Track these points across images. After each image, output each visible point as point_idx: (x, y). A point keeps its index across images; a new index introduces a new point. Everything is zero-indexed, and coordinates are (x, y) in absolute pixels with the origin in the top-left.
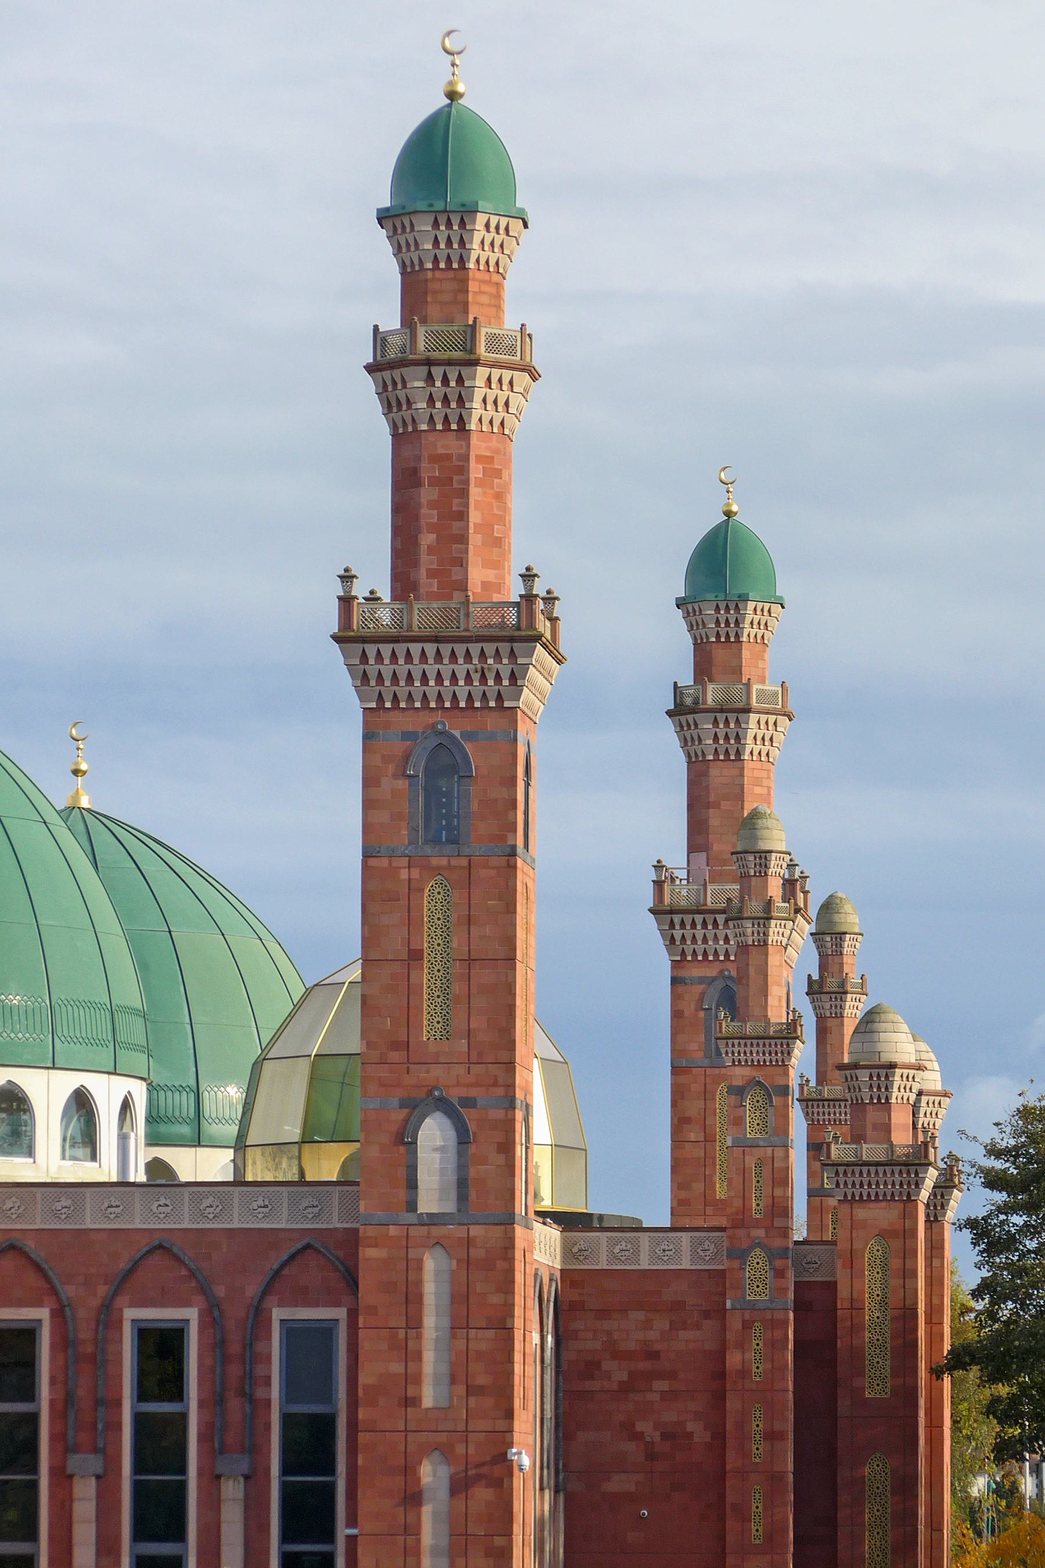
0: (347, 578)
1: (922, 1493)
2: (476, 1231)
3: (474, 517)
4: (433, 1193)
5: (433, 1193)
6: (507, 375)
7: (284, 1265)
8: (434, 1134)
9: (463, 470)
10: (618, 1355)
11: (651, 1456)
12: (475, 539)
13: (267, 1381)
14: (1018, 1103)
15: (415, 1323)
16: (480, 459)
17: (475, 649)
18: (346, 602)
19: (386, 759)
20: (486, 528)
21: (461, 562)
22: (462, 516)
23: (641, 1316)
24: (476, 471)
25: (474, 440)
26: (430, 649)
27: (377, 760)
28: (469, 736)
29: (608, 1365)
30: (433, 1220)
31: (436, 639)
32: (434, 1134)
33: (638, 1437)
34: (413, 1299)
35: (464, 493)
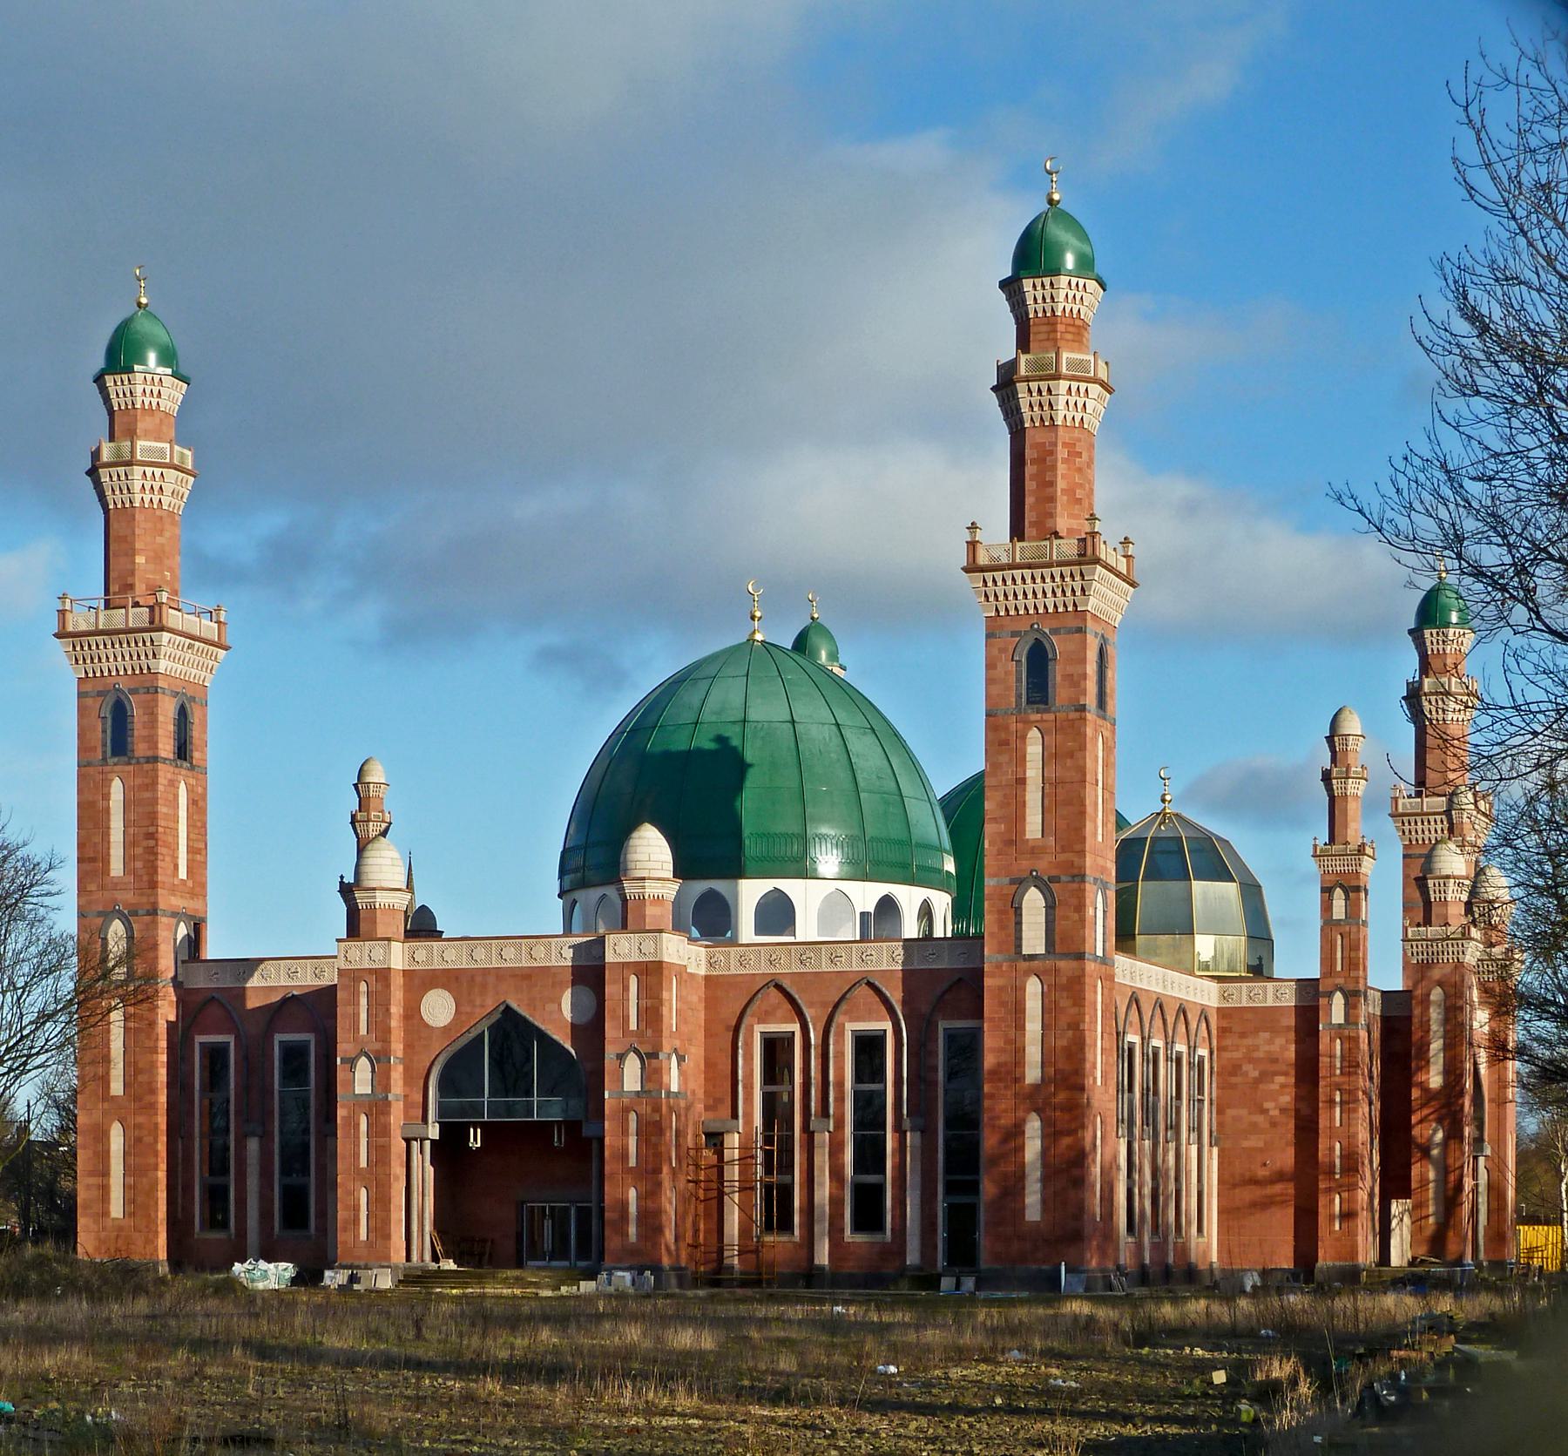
0: (973, 527)
1: (941, 1234)
2: (1062, 964)
3: (1061, 484)
4: (1034, 940)
5: (1034, 940)
6: (1083, 386)
7: (944, 993)
8: (1033, 901)
9: (1052, 453)
10: (1251, 1060)
11: (1274, 1124)
12: (1062, 499)
13: (935, 1069)
14: (179, 353)
15: (1020, 1026)
16: (1065, 445)
17: (1056, 571)
18: (973, 545)
19: (1002, 650)
20: (1070, 492)
21: (1052, 515)
22: (1052, 484)
23: (1267, 1035)
24: (1062, 453)
25: (1061, 432)
26: (1027, 573)
27: (996, 652)
28: (1055, 631)
29: (1247, 1067)
30: (1032, 957)
31: (1029, 567)
32: (1033, 901)
33: (1264, 1112)
34: (1019, 1010)
35: (1054, 468)
